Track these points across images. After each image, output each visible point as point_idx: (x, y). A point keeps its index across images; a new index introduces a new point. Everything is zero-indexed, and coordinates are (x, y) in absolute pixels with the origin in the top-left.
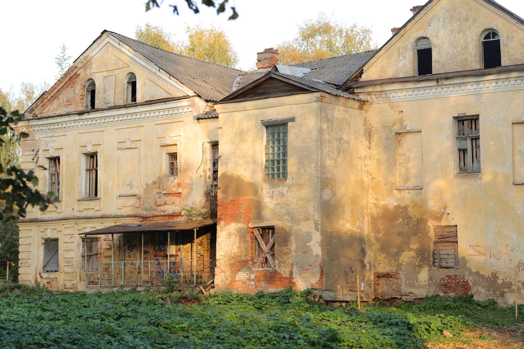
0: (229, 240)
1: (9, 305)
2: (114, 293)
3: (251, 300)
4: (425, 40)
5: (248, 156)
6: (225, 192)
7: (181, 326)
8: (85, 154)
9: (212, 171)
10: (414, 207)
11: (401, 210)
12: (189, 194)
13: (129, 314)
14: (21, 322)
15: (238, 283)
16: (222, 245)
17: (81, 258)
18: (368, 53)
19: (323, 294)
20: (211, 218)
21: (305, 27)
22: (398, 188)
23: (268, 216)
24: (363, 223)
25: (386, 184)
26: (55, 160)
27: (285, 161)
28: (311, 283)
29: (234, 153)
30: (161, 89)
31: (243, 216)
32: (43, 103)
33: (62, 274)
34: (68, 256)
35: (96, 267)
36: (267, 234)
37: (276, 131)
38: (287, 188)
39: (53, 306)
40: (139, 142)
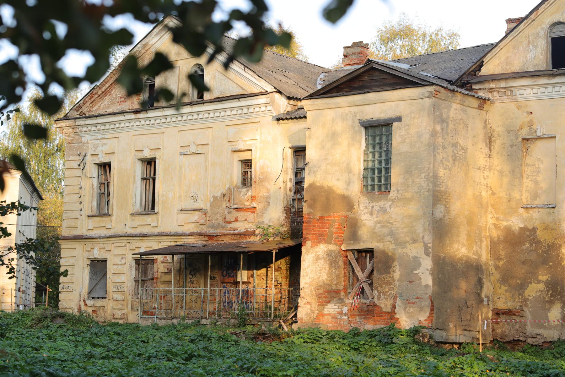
0: (316, 265)
1: (50, 338)
2: (175, 327)
3: (343, 339)
4: (562, 26)
5: (343, 163)
6: (310, 206)
7: (285, 373)
8: (141, 160)
9: (293, 181)
10: (545, 229)
11: (528, 233)
12: (265, 209)
13: (202, 353)
14: (69, 362)
15: (326, 317)
16: (308, 270)
17: (134, 283)
18: (477, 48)
19: (434, 334)
20: (292, 239)
21: (384, 29)
22: (524, 206)
23: (365, 236)
24: (480, 248)
25: (509, 201)
26: (105, 167)
27: (388, 170)
28: (418, 319)
29: (325, 159)
30: (234, 84)
31: (335, 236)
32: (93, 100)
33: (110, 301)
34: (118, 280)
35: (151, 293)
36: (363, 258)
37: (378, 133)
38: (390, 203)
39: (104, 340)
40: (206, 147)
